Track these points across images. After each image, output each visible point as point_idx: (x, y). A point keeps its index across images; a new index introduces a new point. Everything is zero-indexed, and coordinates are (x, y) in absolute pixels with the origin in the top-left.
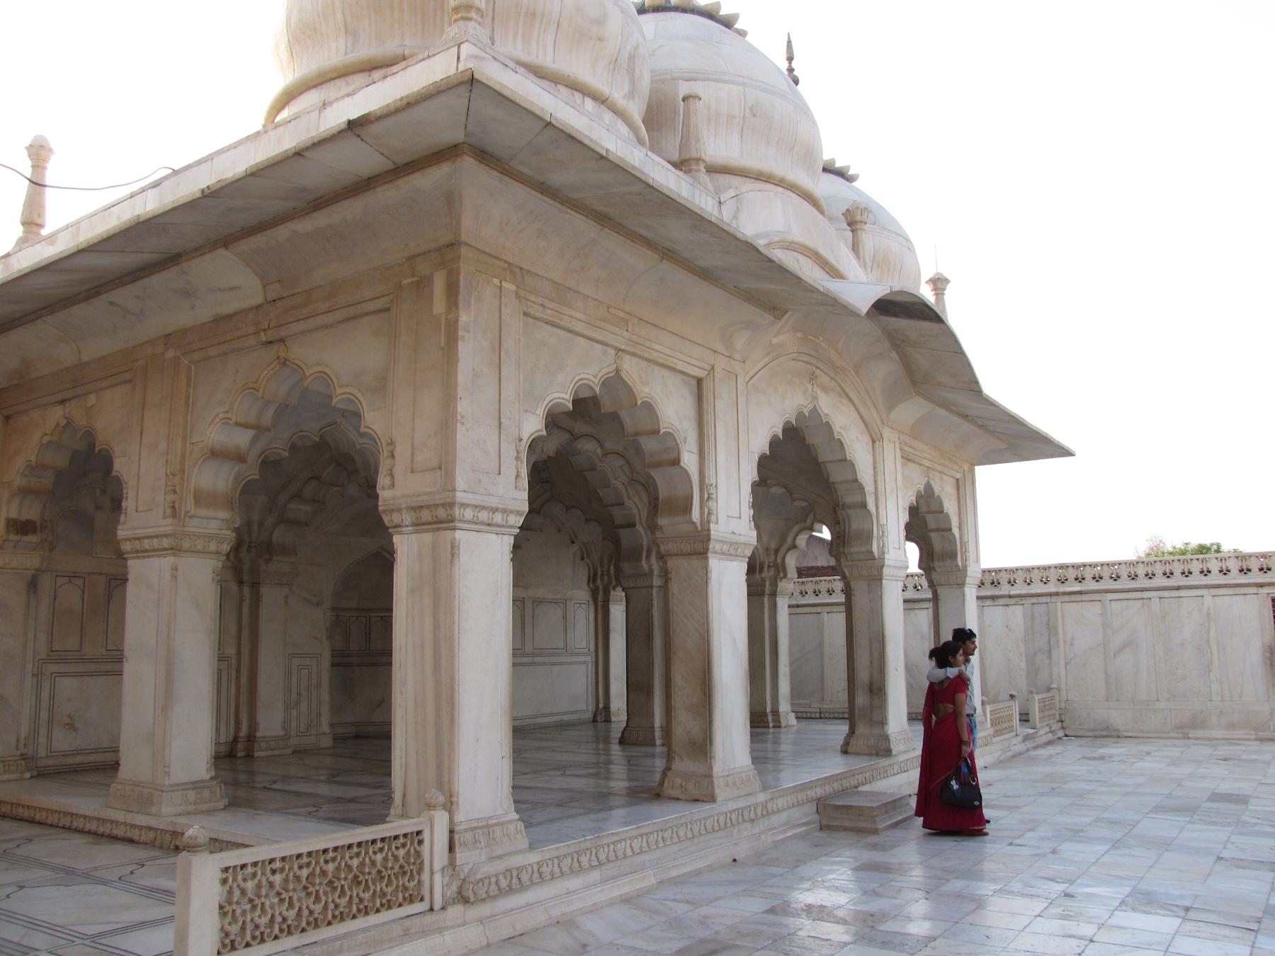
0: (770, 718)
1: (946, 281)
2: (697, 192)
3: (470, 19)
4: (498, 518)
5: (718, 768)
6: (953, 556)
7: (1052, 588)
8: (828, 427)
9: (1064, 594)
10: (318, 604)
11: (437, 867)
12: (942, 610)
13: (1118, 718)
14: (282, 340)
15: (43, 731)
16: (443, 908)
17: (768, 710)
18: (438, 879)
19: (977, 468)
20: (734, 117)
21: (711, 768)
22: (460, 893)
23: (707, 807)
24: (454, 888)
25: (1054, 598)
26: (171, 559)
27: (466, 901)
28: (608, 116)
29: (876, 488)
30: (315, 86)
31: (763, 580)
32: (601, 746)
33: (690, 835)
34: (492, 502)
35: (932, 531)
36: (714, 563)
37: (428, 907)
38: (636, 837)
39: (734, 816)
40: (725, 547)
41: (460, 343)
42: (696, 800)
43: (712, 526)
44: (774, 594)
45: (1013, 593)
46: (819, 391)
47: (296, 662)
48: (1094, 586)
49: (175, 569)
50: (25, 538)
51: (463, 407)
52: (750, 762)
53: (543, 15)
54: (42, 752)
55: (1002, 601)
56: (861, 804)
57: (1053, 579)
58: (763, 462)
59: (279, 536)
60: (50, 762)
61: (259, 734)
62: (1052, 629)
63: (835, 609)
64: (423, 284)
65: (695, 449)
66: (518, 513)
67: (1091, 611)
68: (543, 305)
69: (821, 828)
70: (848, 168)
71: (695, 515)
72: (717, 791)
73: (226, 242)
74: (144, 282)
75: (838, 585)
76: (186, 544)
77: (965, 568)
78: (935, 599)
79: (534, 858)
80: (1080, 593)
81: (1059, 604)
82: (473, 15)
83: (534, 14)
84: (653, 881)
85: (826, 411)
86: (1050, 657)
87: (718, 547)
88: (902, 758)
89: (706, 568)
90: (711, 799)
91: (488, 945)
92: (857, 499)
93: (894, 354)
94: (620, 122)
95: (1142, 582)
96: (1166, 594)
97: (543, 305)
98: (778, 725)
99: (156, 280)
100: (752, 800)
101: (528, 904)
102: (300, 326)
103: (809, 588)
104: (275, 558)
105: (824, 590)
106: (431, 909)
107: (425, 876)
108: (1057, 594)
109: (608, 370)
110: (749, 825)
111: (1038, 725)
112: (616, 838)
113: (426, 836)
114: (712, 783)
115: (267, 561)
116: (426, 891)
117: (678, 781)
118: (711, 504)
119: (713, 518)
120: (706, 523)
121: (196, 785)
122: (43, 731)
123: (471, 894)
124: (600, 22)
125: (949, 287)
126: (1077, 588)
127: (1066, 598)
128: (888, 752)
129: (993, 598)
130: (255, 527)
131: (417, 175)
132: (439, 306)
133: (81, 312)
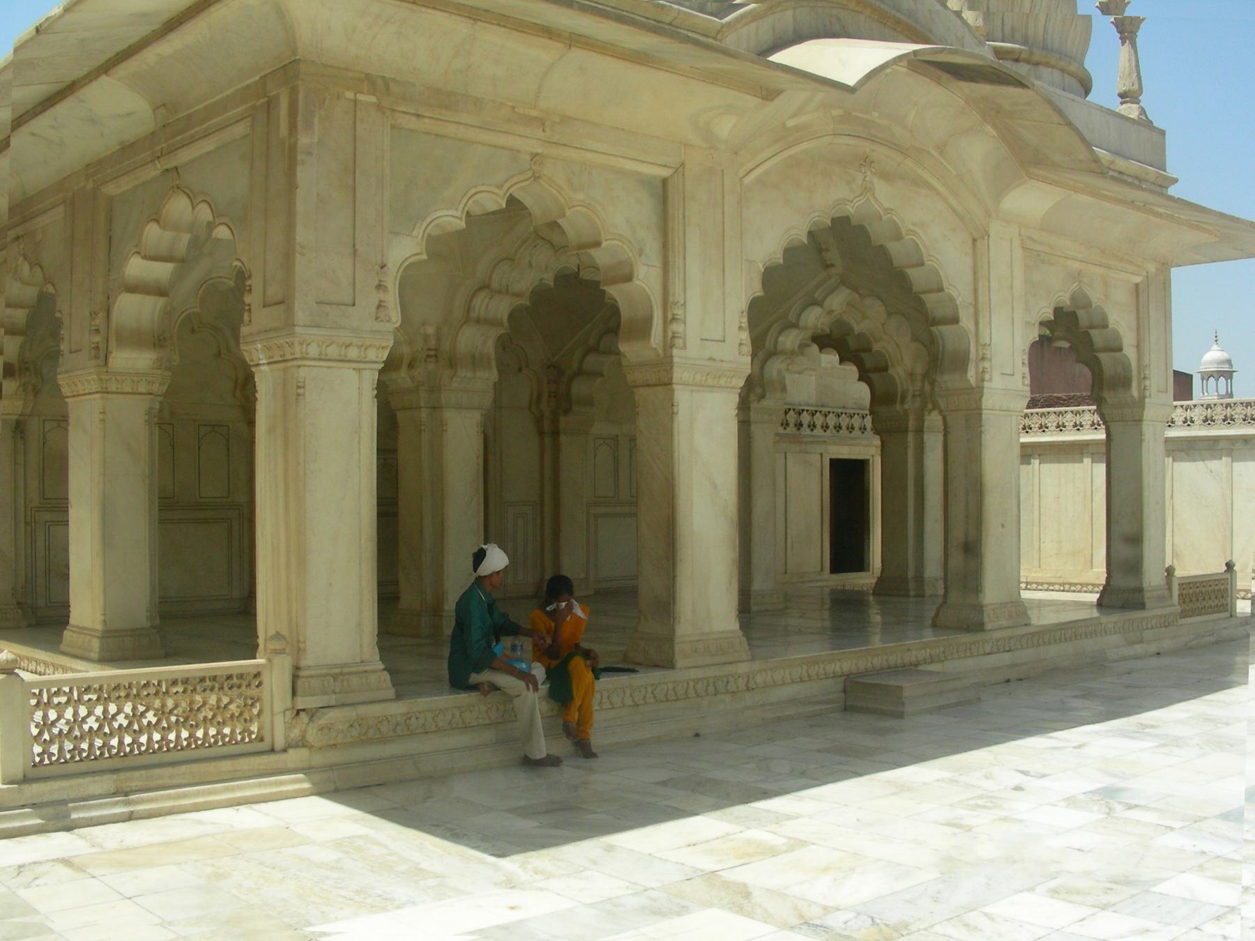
0: (912, 585)
17: (911, 574)
19: (1175, 271)
21: (674, 631)
23: (656, 676)
29: (976, 299)
31: (906, 413)
33: (629, 701)
35: (1100, 351)
36: (682, 396)
39: (699, 686)
41: (299, 168)
43: (675, 352)
44: (920, 431)
46: (875, 180)
51: (302, 235)
52: (737, 626)
58: (770, 276)
64: (270, 105)
65: (657, 262)
68: (418, 116)
69: (845, 709)
73: (106, 68)
74: (50, 113)
85: (887, 205)
88: (998, 635)
90: (669, 664)
97: (418, 116)
98: (920, 595)
99: (61, 109)
103: (1052, 421)
110: (727, 698)
114: (672, 648)
128: (979, 627)
132: (284, 131)
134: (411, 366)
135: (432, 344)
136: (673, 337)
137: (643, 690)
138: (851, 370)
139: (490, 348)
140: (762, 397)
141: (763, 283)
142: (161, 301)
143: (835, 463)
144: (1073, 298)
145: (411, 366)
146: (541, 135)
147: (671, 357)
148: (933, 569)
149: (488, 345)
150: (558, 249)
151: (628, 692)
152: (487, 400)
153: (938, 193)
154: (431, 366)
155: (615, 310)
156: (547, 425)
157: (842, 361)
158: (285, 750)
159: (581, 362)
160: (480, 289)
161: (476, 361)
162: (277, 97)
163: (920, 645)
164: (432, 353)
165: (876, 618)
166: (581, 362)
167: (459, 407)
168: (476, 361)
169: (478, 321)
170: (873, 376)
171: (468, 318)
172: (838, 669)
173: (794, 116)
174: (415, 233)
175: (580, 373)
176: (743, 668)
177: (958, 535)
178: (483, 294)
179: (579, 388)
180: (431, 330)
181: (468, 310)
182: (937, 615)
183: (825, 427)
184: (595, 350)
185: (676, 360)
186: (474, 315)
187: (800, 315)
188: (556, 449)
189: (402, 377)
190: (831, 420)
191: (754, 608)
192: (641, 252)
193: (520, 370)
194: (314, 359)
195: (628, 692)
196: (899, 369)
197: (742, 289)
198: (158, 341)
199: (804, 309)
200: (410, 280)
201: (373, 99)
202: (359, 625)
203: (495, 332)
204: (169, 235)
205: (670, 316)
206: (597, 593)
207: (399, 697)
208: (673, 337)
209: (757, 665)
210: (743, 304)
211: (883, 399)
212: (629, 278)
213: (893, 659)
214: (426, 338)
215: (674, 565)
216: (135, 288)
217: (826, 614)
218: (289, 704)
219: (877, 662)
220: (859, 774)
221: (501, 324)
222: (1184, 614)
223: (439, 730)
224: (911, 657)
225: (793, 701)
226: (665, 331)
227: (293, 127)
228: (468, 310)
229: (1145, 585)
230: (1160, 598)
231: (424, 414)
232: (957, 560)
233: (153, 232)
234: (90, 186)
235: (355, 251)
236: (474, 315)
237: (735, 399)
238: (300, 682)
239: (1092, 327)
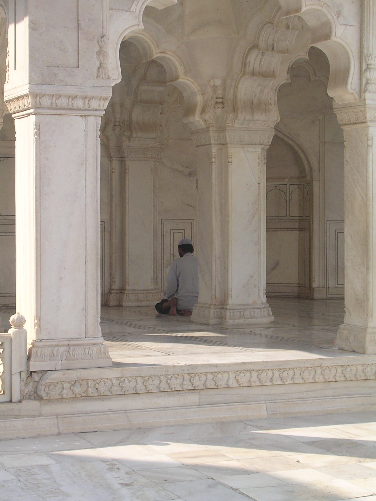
10: (190, 175)
16: (20, 402)
22: (36, 392)
24: (30, 387)
27: (39, 398)
34: (71, 90)
37: (8, 399)
42: (354, 351)
47: (168, 227)
59: (138, 115)
61: (230, 302)
65: (354, 21)
91: (59, 434)
101: (110, 410)
104: (134, 135)
106: (11, 401)
115: (129, 138)
117: (345, 332)
118: (368, 74)
123: (43, 394)
130: (118, 108)
134: (203, 111)
135: (220, 93)
136: (367, 83)
137: (334, 371)
145: (203, 111)
147: (365, 100)
149: (268, 92)
151: (319, 371)
154: (219, 111)
158: (20, 402)
160: (252, 48)
161: (254, 106)
164: (220, 100)
168: (254, 106)
169: (253, 74)
174: (133, 9)
180: (218, 82)
181: (244, 65)
185: (367, 102)
186: (249, 69)
192: (339, 14)
194: (48, 108)
195: (319, 371)
202: (85, 309)
205: (364, 67)
208: (367, 83)
212: (327, 36)
214: (215, 88)
218: (24, 368)
220: (308, 427)
226: (361, 79)
228: (244, 65)
235: (78, 25)
236: (249, 69)
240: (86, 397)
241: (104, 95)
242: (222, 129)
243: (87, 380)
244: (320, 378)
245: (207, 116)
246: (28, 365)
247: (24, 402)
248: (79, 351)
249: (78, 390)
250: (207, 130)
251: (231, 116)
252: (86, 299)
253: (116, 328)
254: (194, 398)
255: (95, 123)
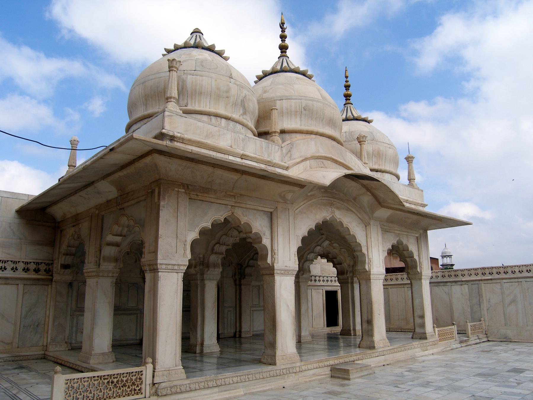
0: (352, 332)
1: (413, 158)
2: (270, 145)
3: (171, 101)
4: (176, 267)
5: (279, 353)
6: (416, 267)
7: (479, 277)
8: (341, 224)
9: (485, 280)
11: (148, 383)
12: (414, 289)
13: (510, 334)
14: (123, 208)
15: (74, 335)
17: (352, 329)
18: (148, 387)
19: (429, 232)
20: (297, 112)
21: (276, 353)
23: (270, 368)
24: (154, 390)
25: (481, 282)
26: (96, 279)
27: (158, 395)
28: (232, 124)
30: (135, 123)
31: (348, 277)
32: (238, 345)
34: (174, 262)
36: (277, 278)
38: (235, 377)
40: (282, 272)
43: (275, 265)
44: (352, 283)
45: (463, 280)
48: (497, 276)
49: (97, 282)
50: (66, 270)
51: (161, 232)
53: (204, 93)
54: (73, 342)
55: (459, 283)
56: (344, 368)
57: (480, 273)
58: (304, 240)
60: (76, 345)
62: (480, 295)
63: (407, 286)
64: (153, 192)
65: (269, 237)
66: (184, 265)
67: (497, 287)
69: (331, 377)
70: (368, 118)
71: (269, 260)
72: (277, 361)
73: (104, 177)
75: (405, 276)
76: (101, 274)
77: (421, 273)
78: (411, 284)
79: (187, 382)
80: (491, 279)
81: (483, 284)
82: (172, 100)
83: (201, 93)
84: (242, 393)
86: (480, 307)
87: (278, 272)
88: (379, 350)
89: (274, 279)
90: (274, 364)
92: (359, 249)
93: (369, 193)
94: (237, 125)
95: (518, 275)
96: (528, 280)
97: (197, 195)
100: (294, 365)
102: (126, 204)
105: (400, 278)
107: (143, 386)
108: (482, 280)
109: (229, 214)
111: (470, 336)
112: (225, 377)
113: (144, 373)
114: (275, 358)
116: (143, 391)
119: (276, 261)
120: (273, 264)
121: (104, 354)
122: (74, 335)
124: (228, 91)
125: (414, 160)
126: (490, 277)
127: (486, 282)
129: (456, 282)
131: (143, 159)
132: (156, 200)
133: (73, 198)
135: (202, 260)
138: (331, 264)
139: (220, 261)
140: (303, 274)
141: (335, 180)
142: (118, 248)
143: (327, 292)
144: (397, 242)
145: (195, 267)
146: (234, 200)
148: (358, 327)
150: (240, 232)
152: (219, 277)
153: (354, 213)
154: (201, 267)
155: (256, 250)
156: (237, 283)
157: (328, 261)
159: (248, 263)
162: (154, 190)
163: (355, 354)
165: (342, 344)
166: (248, 263)
167: (210, 279)
168: (215, 266)
169: (216, 253)
170: (337, 266)
171: (213, 252)
172: (328, 364)
173: (309, 192)
175: (248, 266)
176: (298, 364)
177: (365, 318)
178: (218, 245)
179: (248, 271)
180: (201, 256)
182: (360, 344)
183: (323, 281)
184: (252, 259)
186: (215, 251)
187: (303, 265)
188: (240, 290)
189: (192, 271)
190: (325, 279)
191: (302, 341)
192: (264, 234)
193: (229, 265)
196: (345, 264)
197: (295, 244)
198: (116, 260)
199: (315, 247)
200: (194, 244)
201: (184, 191)
202: (175, 354)
203: (221, 257)
204: (120, 229)
206: (253, 335)
207: (188, 378)
209: (303, 363)
210: (296, 250)
211: (340, 273)
213: (347, 360)
214: (200, 258)
215: (275, 331)
216: (109, 244)
217: (326, 343)
218: (151, 382)
219: (341, 361)
221: (222, 254)
222: (440, 340)
223: (200, 389)
224: (352, 359)
225: (314, 375)
227: (159, 199)
229: (427, 332)
230: (432, 336)
231: (199, 282)
232: (365, 325)
233: (116, 229)
234: (97, 212)
237: (293, 278)
238: (155, 373)
239: (404, 251)
240: (176, 393)
241: (185, 264)
242: (202, 274)
243: (177, 386)
244: (261, 377)
245: (197, 269)
246: (153, 380)
247: (151, 397)
248: (173, 372)
249: (173, 390)
250: (196, 274)
251: (207, 269)
252: (176, 350)
253: (191, 364)
254: (216, 390)
255: (181, 275)
